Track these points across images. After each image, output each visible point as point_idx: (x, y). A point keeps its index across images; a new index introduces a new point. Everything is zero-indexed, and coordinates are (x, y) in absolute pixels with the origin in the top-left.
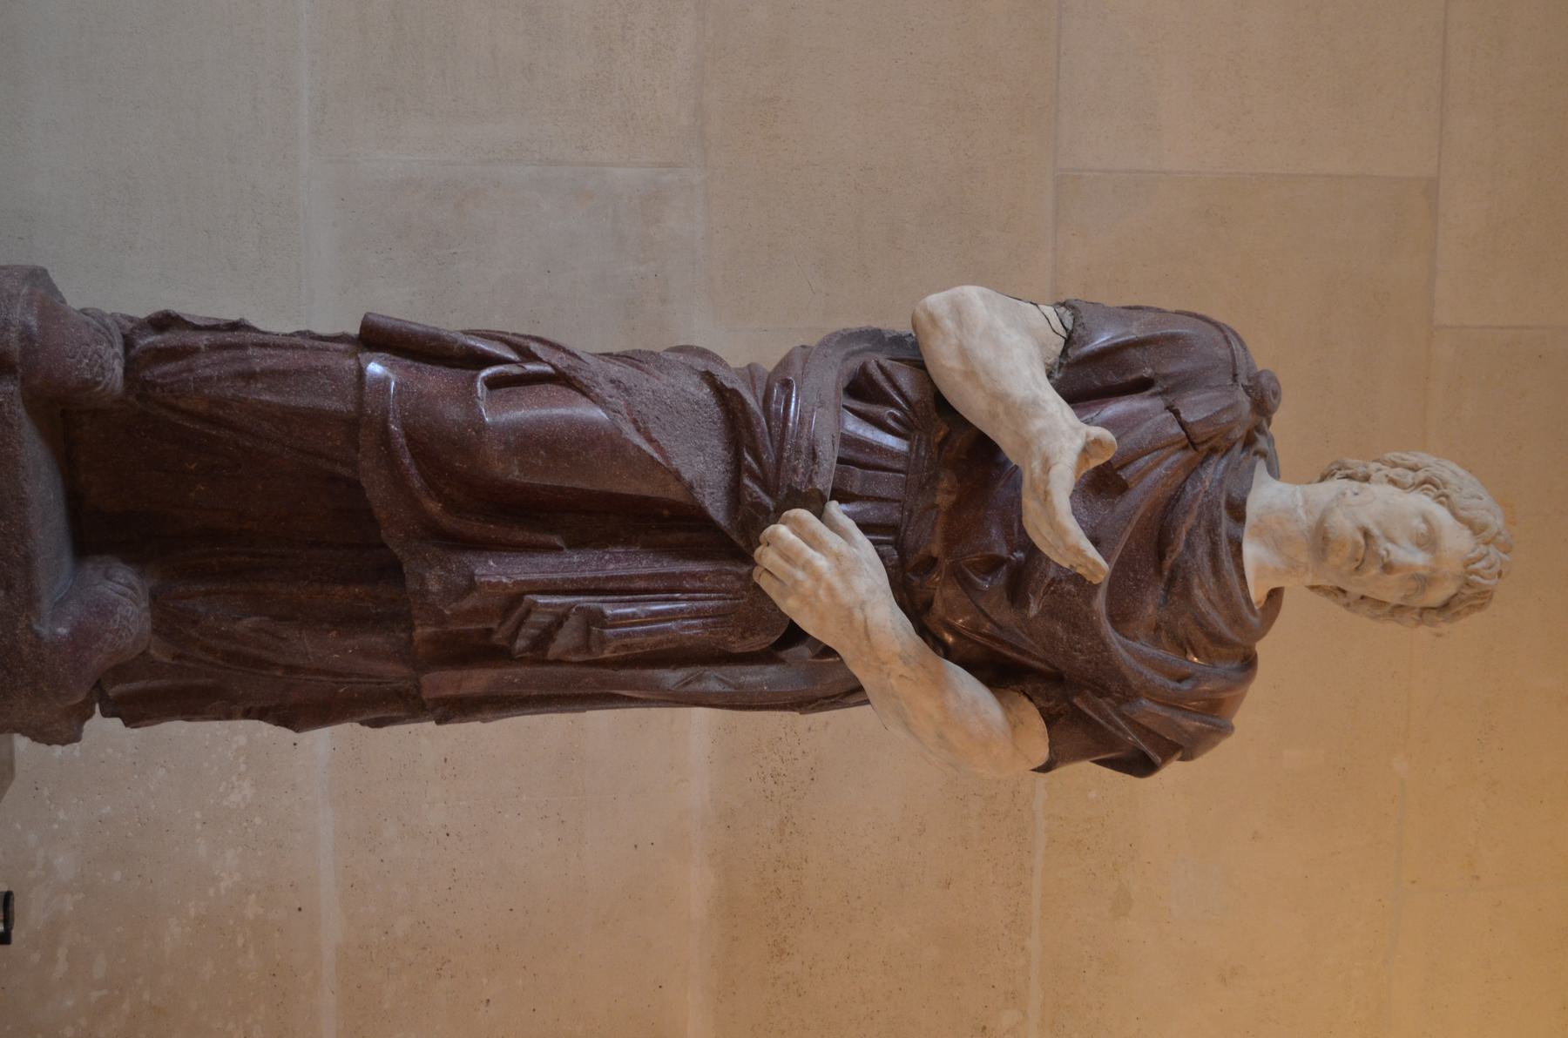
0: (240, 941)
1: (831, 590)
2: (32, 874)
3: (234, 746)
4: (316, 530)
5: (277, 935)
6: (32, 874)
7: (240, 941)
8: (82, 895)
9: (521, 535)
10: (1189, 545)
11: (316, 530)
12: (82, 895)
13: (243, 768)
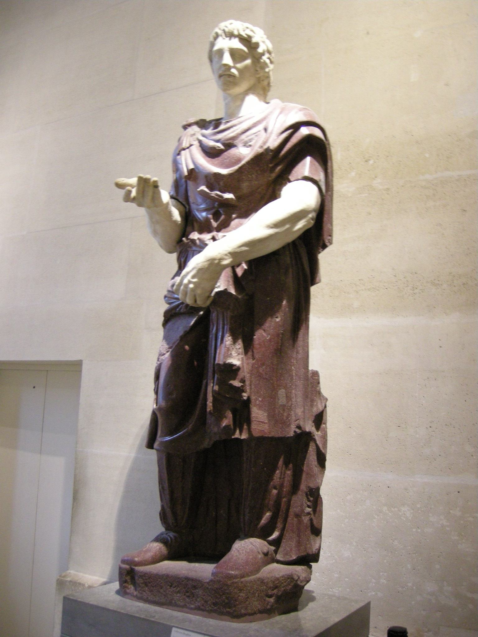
0: (471, 519)
1: (193, 277)
2: (434, 601)
3: (387, 512)
4: (229, 462)
5: (469, 503)
6: (434, 601)
7: (471, 519)
8: (445, 582)
9: (203, 387)
10: (218, 141)
11: (229, 462)
12: (445, 582)
13: (396, 509)
